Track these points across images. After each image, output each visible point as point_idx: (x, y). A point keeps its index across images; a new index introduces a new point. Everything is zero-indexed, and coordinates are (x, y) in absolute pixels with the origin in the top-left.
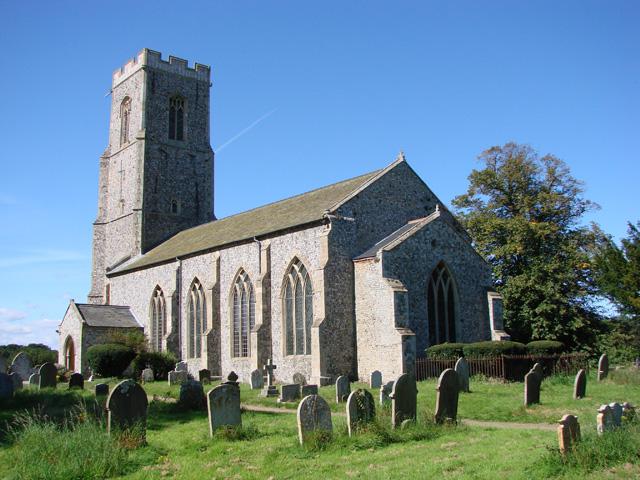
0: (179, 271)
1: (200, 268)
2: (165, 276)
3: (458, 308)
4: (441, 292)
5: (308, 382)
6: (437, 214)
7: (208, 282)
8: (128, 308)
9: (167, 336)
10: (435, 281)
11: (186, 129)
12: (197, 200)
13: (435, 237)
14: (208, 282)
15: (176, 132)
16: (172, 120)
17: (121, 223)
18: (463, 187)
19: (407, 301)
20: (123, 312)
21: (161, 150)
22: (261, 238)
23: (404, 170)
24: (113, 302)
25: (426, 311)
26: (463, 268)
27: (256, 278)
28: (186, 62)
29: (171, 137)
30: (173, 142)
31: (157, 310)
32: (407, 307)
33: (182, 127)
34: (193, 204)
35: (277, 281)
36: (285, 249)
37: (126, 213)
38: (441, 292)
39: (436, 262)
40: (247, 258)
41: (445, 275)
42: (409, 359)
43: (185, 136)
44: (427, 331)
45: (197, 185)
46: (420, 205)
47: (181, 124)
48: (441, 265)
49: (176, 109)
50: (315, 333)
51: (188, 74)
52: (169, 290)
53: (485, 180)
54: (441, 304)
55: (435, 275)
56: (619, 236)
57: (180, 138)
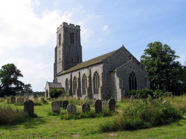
0: (71, 75)
1: (76, 74)
2: (68, 76)
3: (137, 83)
4: (133, 79)
5: (29, 98)
6: (132, 60)
7: (77, 77)
8: (61, 83)
9: (87, 88)
10: (134, 77)
11: (75, 41)
12: (78, 58)
13: (131, 65)
14: (77, 77)
15: (72, 41)
16: (71, 39)
17: (60, 64)
18: (142, 53)
19: (122, 82)
20: (60, 84)
21: (68, 47)
22: (88, 67)
23: (123, 49)
24: (58, 82)
25: (128, 84)
26: (139, 73)
27: (87, 76)
28: (67, 23)
29: (71, 43)
30: (71, 44)
31: (67, 84)
32: (122, 83)
33: (74, 41)
34: (77, 59)
35: (92, 77)
36: (94, 69)
37: (61, 61)
38: (133, 79)
39: (131, 72)
40: (86, 72)
41: (134, 75)
42: (123, 96)
43: (75, 42)
44: (129, 89)
45: (78, 54)
46: (128, 58)
47: (73, 40)
48: (133, 73)
49: (72, 36)
50: (100, 89)
51: (75, 28)
52: (69, 79)
53: (148, 51)
54: (133, 82)
55: (131, 75)
56: (183, 64)
57: (73, 43)
